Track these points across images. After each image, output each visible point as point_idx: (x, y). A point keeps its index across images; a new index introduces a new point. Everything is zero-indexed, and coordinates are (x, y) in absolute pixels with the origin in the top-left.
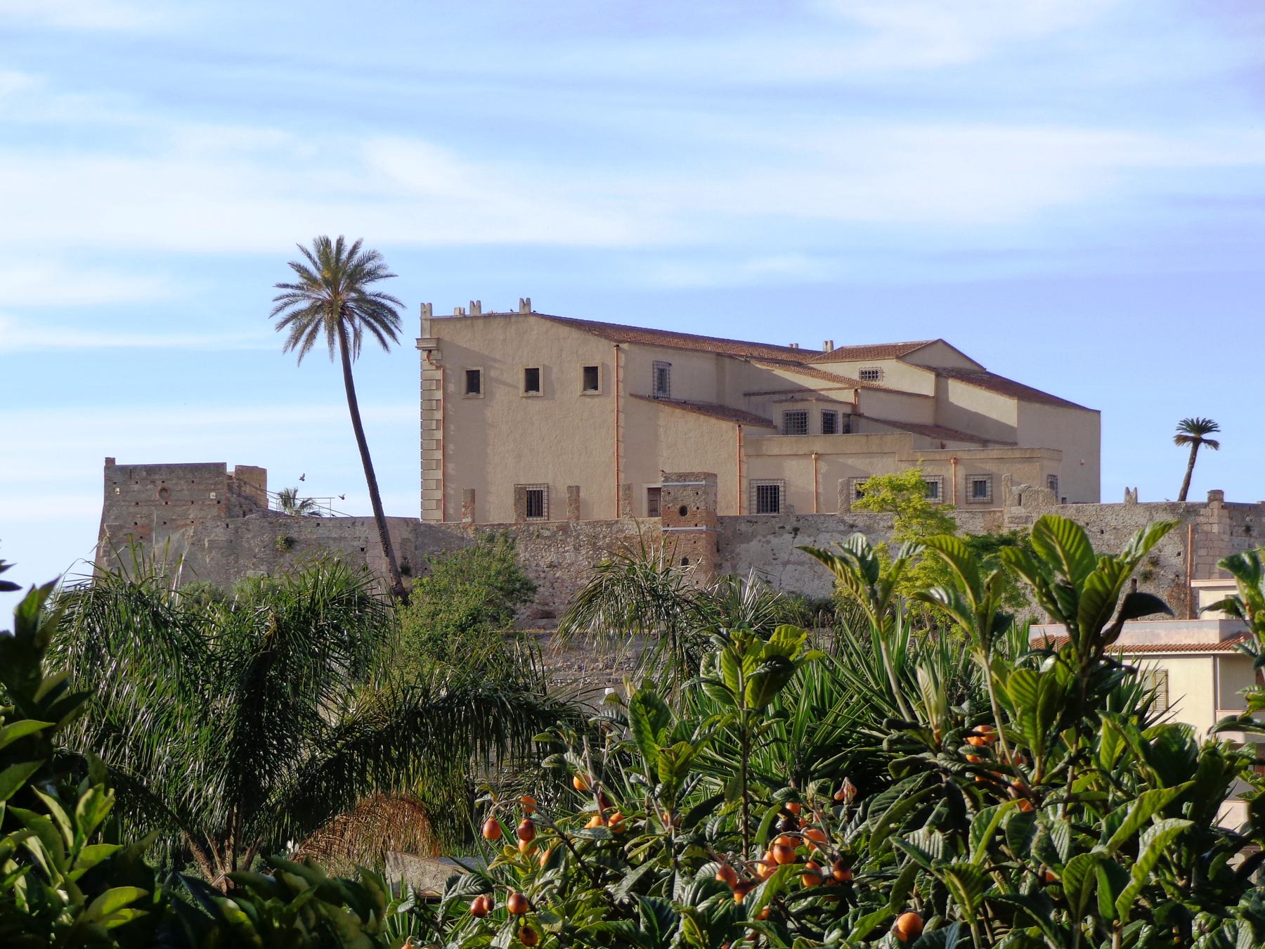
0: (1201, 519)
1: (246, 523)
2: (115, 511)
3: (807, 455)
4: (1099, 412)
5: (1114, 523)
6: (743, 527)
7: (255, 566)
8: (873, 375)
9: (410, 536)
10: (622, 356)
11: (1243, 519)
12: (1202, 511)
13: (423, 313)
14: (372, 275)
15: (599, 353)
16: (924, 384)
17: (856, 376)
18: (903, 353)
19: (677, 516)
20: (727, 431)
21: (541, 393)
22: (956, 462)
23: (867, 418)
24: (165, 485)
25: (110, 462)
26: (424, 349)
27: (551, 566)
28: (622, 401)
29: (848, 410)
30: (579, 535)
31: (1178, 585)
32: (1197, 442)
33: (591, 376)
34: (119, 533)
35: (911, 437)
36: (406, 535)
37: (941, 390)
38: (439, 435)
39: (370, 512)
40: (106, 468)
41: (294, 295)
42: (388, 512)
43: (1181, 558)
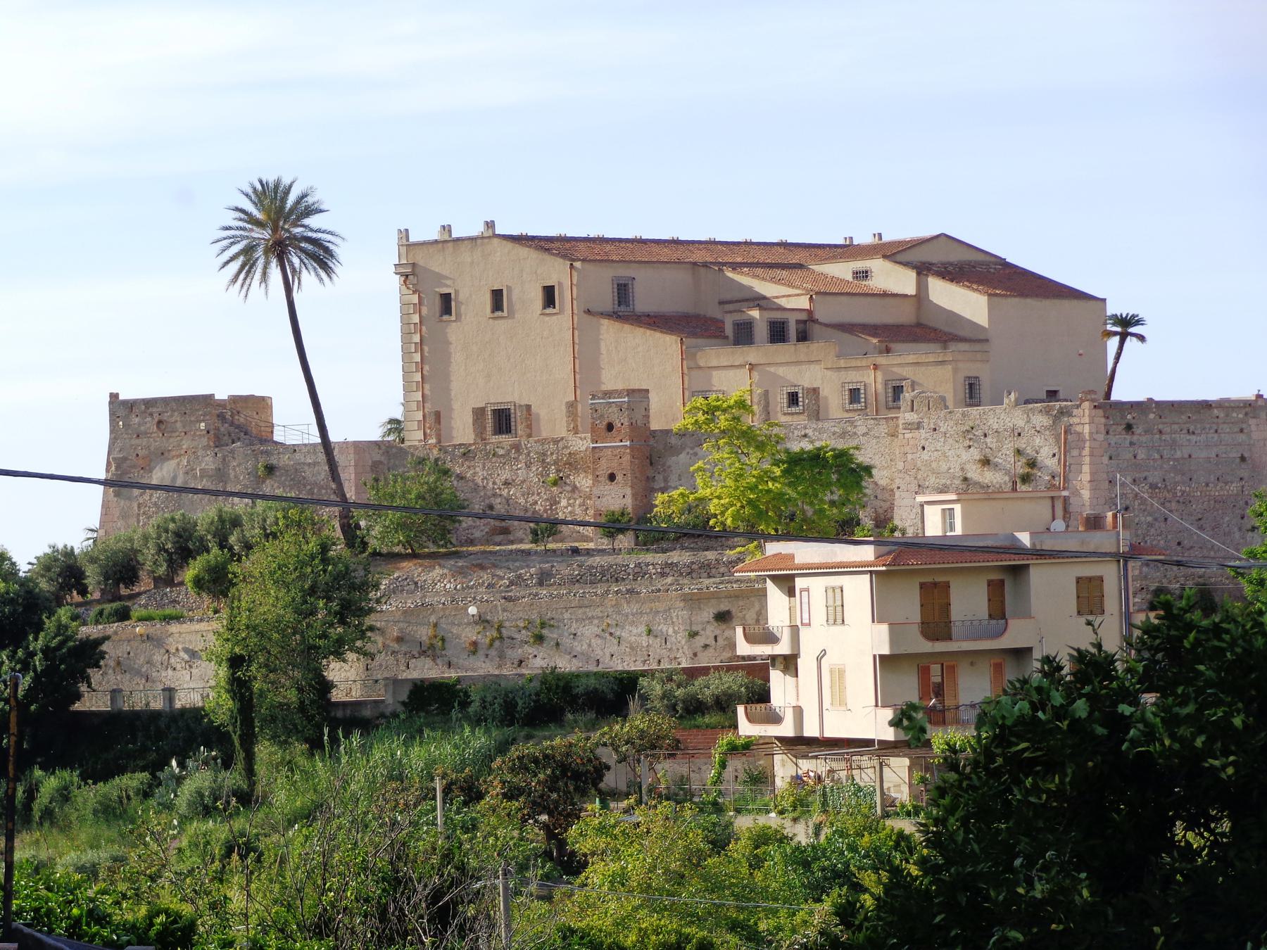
0: (1076, 420)
1: (232, 452)
2: (119, 443)
3: (741, 366)
4: (1104, 300)
5: (995, 426)
6: (673, 441)
8: (863, 275)
10: (575, 274)
11: (1123, 417)
12: (1075, 412)
14: (310, 211)
15: (556, 271)
16: (901, 281)
17: (849, 277)
18: (896, 252)
20: (669, 344)
21: (505, 314)
22: (876, 367)
23: (821, 324)
25: (114, 397)
26: (401, 274)
27: (506, 483)
28: (576, 318)
29: (804, 316)
30: (529, 453)
32: (1124, 337)
33: (549, 296)
35: (962, 333)
36: (377, 457)
38: (417, 357)
39: (317, 440)
40: (110, 403)
41: (233, 237)
42: (334, 437)
43: (1056, 460)
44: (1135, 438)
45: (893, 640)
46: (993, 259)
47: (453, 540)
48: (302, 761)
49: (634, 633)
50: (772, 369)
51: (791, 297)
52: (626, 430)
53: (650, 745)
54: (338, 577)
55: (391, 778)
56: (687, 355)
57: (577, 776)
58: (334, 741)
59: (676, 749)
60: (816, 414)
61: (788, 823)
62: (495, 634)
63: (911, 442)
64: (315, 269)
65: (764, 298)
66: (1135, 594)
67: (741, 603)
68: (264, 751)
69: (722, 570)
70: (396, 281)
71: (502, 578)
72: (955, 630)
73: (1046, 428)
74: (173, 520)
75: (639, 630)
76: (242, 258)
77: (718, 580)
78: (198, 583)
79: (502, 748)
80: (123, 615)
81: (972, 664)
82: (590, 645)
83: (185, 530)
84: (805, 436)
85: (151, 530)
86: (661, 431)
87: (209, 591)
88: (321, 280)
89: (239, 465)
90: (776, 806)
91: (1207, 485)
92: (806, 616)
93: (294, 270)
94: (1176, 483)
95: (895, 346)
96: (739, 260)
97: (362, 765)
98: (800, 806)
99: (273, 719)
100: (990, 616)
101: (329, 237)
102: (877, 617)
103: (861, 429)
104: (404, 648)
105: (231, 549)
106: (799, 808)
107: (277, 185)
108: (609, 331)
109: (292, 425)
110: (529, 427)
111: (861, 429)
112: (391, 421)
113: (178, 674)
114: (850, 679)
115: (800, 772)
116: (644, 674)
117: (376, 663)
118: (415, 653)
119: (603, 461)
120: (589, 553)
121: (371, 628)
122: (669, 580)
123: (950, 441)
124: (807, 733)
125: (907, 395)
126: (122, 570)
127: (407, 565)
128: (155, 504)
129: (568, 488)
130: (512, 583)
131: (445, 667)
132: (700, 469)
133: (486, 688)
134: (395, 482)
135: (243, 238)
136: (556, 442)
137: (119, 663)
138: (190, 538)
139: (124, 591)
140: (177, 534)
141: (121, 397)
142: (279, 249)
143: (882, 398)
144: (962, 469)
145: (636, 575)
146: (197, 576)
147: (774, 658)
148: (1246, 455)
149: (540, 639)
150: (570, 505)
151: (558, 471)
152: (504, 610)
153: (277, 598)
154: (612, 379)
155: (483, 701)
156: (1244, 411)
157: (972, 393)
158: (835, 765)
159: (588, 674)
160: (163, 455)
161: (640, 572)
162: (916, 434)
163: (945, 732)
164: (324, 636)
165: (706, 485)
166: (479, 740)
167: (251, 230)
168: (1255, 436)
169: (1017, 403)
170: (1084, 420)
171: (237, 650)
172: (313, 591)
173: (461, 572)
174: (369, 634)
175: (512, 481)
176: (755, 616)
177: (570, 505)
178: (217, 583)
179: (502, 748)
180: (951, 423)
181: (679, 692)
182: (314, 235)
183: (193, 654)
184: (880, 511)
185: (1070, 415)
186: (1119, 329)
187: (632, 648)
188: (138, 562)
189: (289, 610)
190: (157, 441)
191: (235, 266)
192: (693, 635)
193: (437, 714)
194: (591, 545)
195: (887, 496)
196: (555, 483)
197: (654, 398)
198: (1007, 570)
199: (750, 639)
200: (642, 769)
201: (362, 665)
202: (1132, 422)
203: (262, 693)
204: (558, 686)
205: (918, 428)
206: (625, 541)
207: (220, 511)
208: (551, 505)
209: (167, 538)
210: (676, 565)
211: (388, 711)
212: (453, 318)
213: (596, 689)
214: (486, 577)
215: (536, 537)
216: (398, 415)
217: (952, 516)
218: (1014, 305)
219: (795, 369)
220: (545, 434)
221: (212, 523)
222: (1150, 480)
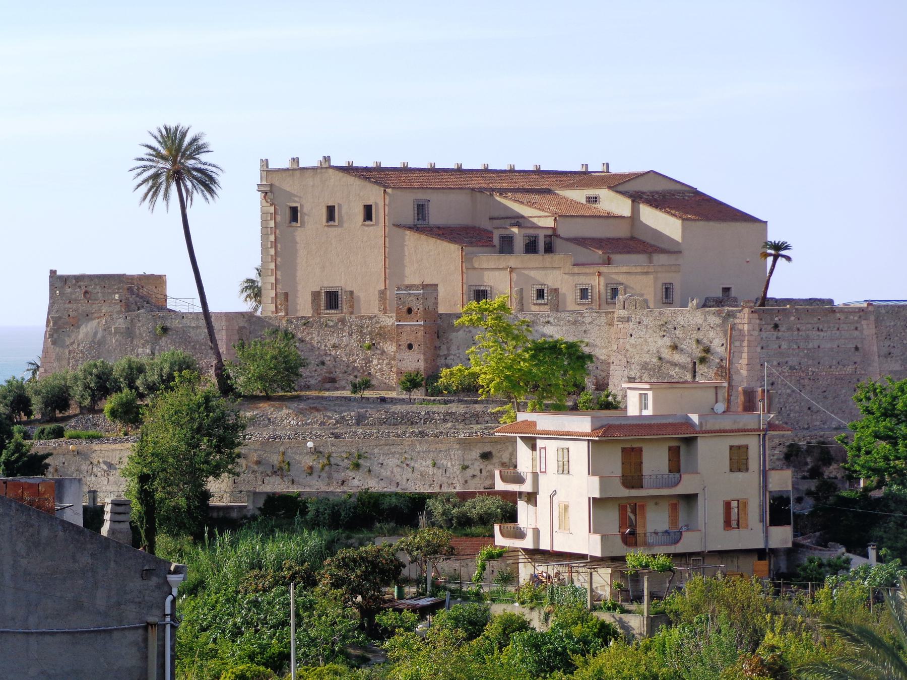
0: (737, 321)
1: (138, 316)
2: (56, 307)
5: (682, 323)
7: (144, 346)
8: (593, 200)
10: (387, 197)
11: (772, 319)
12: (738, 315)
13: (262, 166)
14: (200, 149)
15: (373, 195)
16: (620, 206)
17: (584, 201)
19: (405, 315)
20: (453, 251)
21: (336, 223)
22: (600, 274)
23: (562, 238)
25: (53, 273)
26: (262, 192)
27: (334, 346)
29: (550, 232)
30: (351, 327)
31: (722, 367)
32: (776, 258)
33: (368, 213)
34: (59, 326)
35: (662, 246)
36: (242, 324)
37: (635, 211)
38: (272, 252)
39: (200, 310)
40: (50, 277)
41: (145, 166)
42: (212, 308)
43: (723, 348)
44: (780, 334)
45: (603, 487)
46: (687, 189)
47: (296, 388)
48: (187, 548)
49: (424, 465)
50: (526, 272)
51: (541, 218)
52: (421, 313)
53: (434, 550)
54: (216, 420)
55: (252, 567)
56: (466, 259)
57: (382, 572)
58: (212, 535)
59: (451, 553)
60: (556, 307)
61: (526, 611)
62: (326, 461)
63: (623, 331)
64: (202, 191)
65: (523, 217)
66: (774, 448)
67: (499, 447)
68: (162, 540)
69: (486, 419)
70: (259, 196)
71: (330, 418)
72: (645, 482)
73: (718, 326)
74: (95, 366)
75: (428, 463)
76: (150, 183)
77: (483, 426)
78: (113, 413)
79: (330, 548)
80: (58, 434)
81: (656, 504)
82: (392, 472)
83: (104, 373)
84: (548, 322)
85: (80, 373)
86: (446, 314)
87: (121, 419)
88: (207, 199)
90: (519, 598)
91: (830, 367)
92: (543, 466)
93: (187, 190)
94: (808, 366)
95: (616, 257)
96: (505, 185)
97: (231, 555)
98: (536, 600)
99: (168, 518)
100: (670, 471)
101: (213, 169)
102: (592, 471)
103: (588, 319)
104: (261, 469)
105: (137, 389)
106: (535, 601)
107: (177, 129)
108: (411, 239)
109: (181, 297)
110: (352, 306)
111: (588, 319)
112: (248, 281)
113: (99, 480)
114: (572, 512)
115: (537, 572)
116: (430, 496)
118: (269, 472)
119: (404, 335)
120: (393, 401)
121: (239, 456)
122: (449, 425)
123: (650, 331)
124: (542, 547)
125: (621, 297)
126: (58, 400)
127: (264, 405)
129: (378, 352)
130: (337, 422)
131: (290, 483)
132: (472, 352)
133: (319, 502)
134: (255, 345)
135: (151, 167)
136: (371, 318)
138: (108, 380)
139: (58, 414)
140: (98, 377)
142: (178, 176)
143: (603, 296)
145: (426, 420)
146: (113, 409)
147: (520, 493)
149: (357, 466)
150: (379, 364)
151: (372, 339)
152: (332, 445)
153: (174, 435)
154: (412, 278)
155: (317, 510)
157: (667, 295)
158: (561, 569)
159: (391, 495)
160: (88, 316)
161: (429, 418)
162: (626, 325)
163: (635, 552)
164: (207, 462)
165: (477, 364)
166: (314, 540)
167: (158, 162)
169: (698, 307)
170: (744, 320)
171: (145, 470)
172: (199, 430)
173: (301, 412)
174: (237, 460)
175: (336, 343)
176: (508, 456)
177: (379, 364)
178: (129, 414)
179: (330, 548)
180: (651, 319)
181: (455, 511)
182: (202, 167)
183: (110, 466)
184: (600, 378)
185: (735, 317)
186: (773, 252)
187: (422, 475)
188: (69, 395)
189: (183, 443)
190: (83, 306)
191: (144, 188)
192: (465, 468)
193: (284, 518)
194: (393, 395)
195: (605, 367)
196: (369, 348)
197: (441, 289)
198: (682, 442)
199: (504, 479)
200: (428, 567)
201: (231, 480)
202: (778, 322)
203: (162, 501)
204: (369, 503)
205: (628, 321)
206: (418, 394)
207: (130, 361)
208: (366, 363)
209: (91, 379)
210: (454, 414)
211: (249, 514)
212: (299, 224)
213: (396, 506)
214: (319, 416)
215: (355, 388)
216: (254, 275)
217: (646, 399)
218: (702, 226)
219: (543, 272)
220: (363, 312)
221: (124, 370)
222: (790, 363)
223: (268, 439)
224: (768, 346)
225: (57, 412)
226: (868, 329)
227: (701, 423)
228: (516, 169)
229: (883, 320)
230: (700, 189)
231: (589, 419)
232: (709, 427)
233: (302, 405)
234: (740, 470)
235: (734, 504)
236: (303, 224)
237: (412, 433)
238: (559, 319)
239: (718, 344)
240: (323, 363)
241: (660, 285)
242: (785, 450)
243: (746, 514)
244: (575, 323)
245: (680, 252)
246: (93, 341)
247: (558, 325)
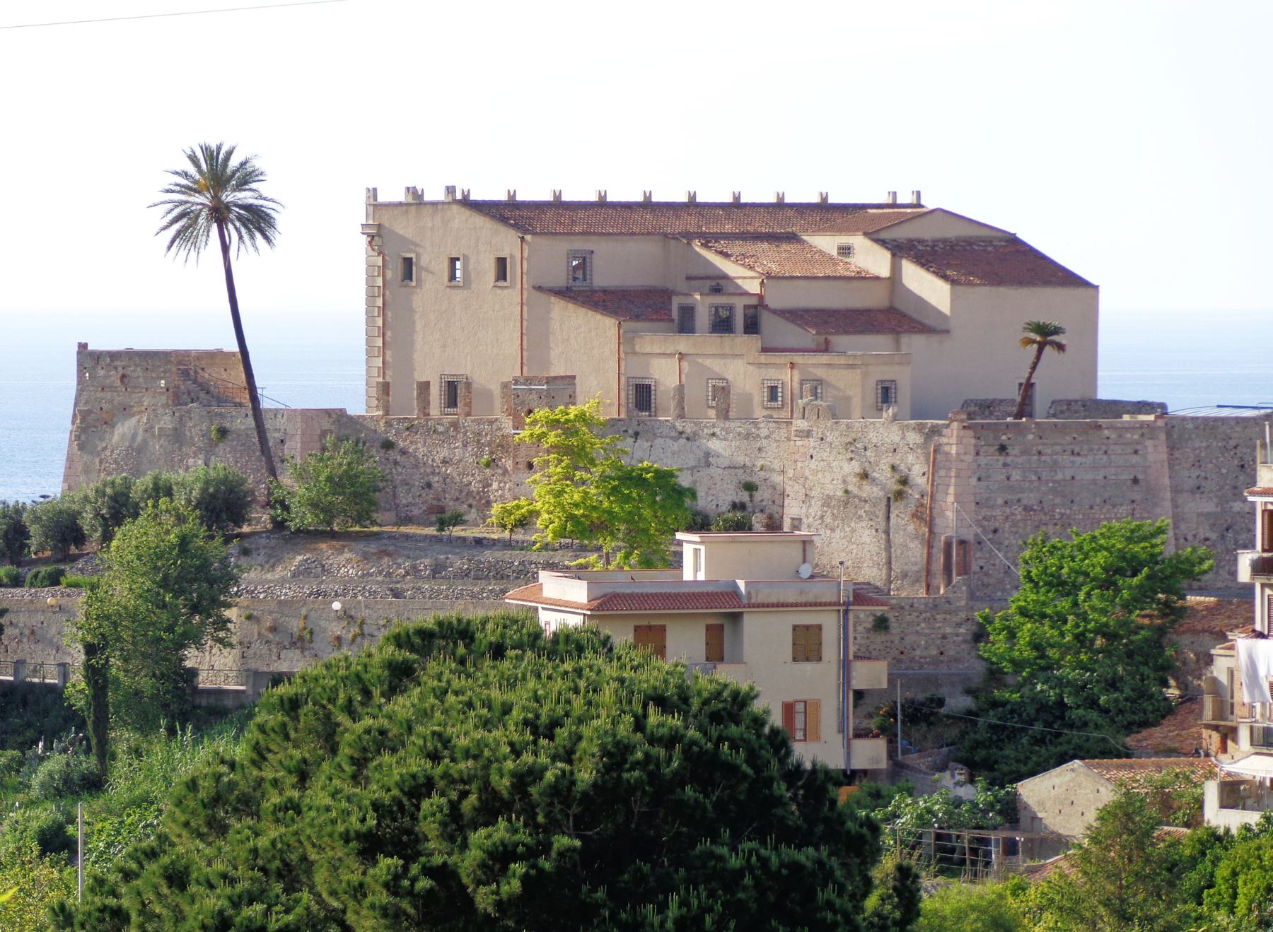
0: (944, 440)
1: (189, 411)
3: (671, 355)
4: (1096, 287)
7: (195, 455)
9: (333, 427)
10: (525, 247)
11: (997, 438)
12: (945, 431)
15: (507, 242)
16: (872, 259)
17: (834, 253)
20: (604, 328)
22: (793, 366)
24: (125, 372)
25: (83, 347)
27: (444, 462)
29: (754, 301)
30: (465, 434)
34: (90, 424)
35: (927, 322)
36: (326, 426)
38: (379, 322)
40: (79, 353)
43: (925, 479)
44: (1009, 459)
46: (999, 234)
50: (700, 360)
56: (626, 342)
62: (358, 630)
63: (802, 450)
70: (364, 240)
73: (918, 446)
84: (713, 434)
89: (195, 426)
91: (1091, 507)
94: (1055, 506)
95: (840, 341)
100: (707, 659)
103: (764, 432)
111: (764, 432)
117: (251, 651)
118: (286, 644)
120: (494, 543)
128: (116, 461)
129: (500, 471)
135: (186, 202)
136: (491, 423)
137: (33, 632)
141: (90, 348)
142: (219, 214)
144: (844, 481)
148: (1140, 477)
150: (500, 488)
151: (491, 453)
156: (1140, 432)
160: (126, 411)
162: (806, 442)
168: (1151, 458)
173: (366, 557)
177: (500, 488)
180: (837, 434)
185: (940, 435)
196: (488, 465)
202: (1007, 442)
205: (807, 437)
212: (414, 284)
218: (983, 296)
223: (310, 595)
224: (989, 477)
225: (73, 547)
226: (1156, 452)
227: (749, 593)
228: (787, 200)
229: (1190, 438)
230: (1020, 236)
231: (584, 584)
232: (761, 598)
233: (373, 547)
234: (808, 660)
235: (800, 707)
236: (419, 281)
237: (491, 591)
238: (727, 431)
239: (918, 472)
240: (429, 485)
241: (871, 383)
242: (974, 628)
243: (818, 723)
244: (747, 436)
245: (948, 332)
246: (130, 446)
247: (725, 439)
